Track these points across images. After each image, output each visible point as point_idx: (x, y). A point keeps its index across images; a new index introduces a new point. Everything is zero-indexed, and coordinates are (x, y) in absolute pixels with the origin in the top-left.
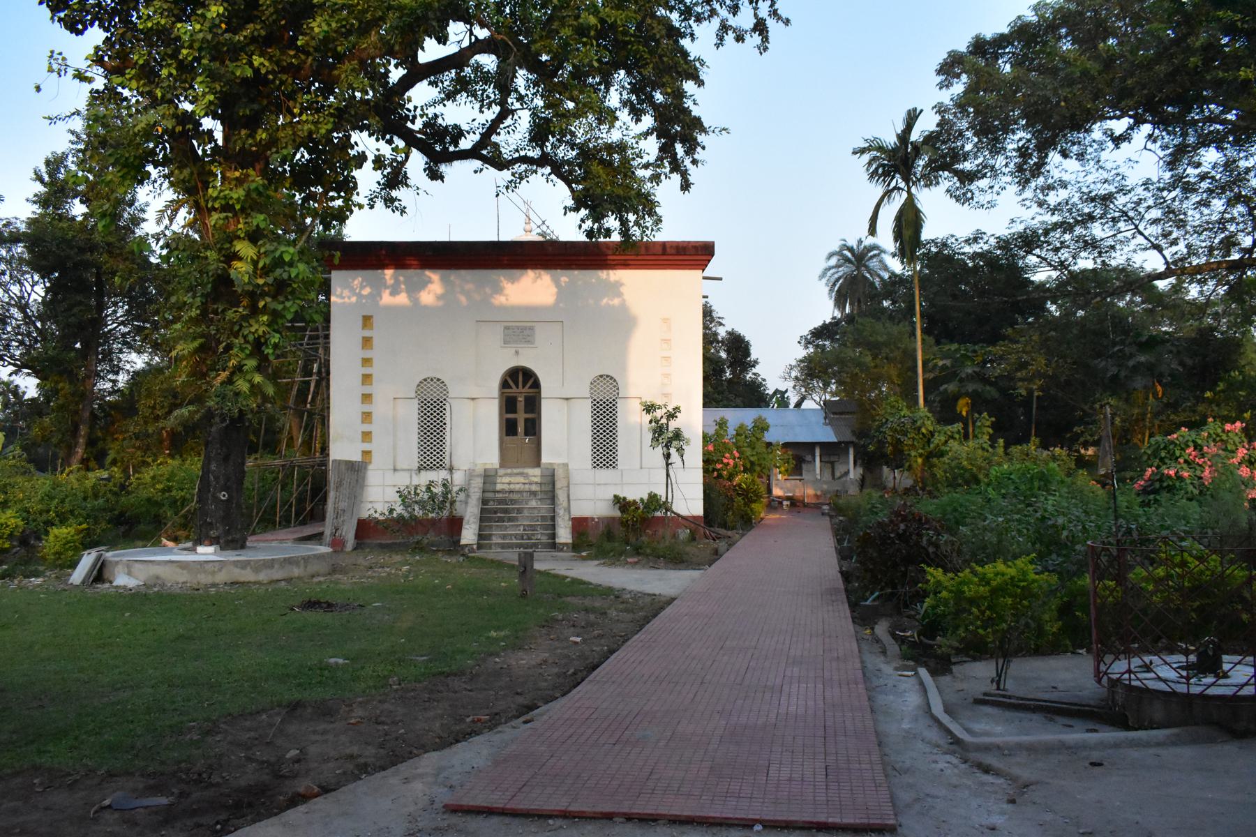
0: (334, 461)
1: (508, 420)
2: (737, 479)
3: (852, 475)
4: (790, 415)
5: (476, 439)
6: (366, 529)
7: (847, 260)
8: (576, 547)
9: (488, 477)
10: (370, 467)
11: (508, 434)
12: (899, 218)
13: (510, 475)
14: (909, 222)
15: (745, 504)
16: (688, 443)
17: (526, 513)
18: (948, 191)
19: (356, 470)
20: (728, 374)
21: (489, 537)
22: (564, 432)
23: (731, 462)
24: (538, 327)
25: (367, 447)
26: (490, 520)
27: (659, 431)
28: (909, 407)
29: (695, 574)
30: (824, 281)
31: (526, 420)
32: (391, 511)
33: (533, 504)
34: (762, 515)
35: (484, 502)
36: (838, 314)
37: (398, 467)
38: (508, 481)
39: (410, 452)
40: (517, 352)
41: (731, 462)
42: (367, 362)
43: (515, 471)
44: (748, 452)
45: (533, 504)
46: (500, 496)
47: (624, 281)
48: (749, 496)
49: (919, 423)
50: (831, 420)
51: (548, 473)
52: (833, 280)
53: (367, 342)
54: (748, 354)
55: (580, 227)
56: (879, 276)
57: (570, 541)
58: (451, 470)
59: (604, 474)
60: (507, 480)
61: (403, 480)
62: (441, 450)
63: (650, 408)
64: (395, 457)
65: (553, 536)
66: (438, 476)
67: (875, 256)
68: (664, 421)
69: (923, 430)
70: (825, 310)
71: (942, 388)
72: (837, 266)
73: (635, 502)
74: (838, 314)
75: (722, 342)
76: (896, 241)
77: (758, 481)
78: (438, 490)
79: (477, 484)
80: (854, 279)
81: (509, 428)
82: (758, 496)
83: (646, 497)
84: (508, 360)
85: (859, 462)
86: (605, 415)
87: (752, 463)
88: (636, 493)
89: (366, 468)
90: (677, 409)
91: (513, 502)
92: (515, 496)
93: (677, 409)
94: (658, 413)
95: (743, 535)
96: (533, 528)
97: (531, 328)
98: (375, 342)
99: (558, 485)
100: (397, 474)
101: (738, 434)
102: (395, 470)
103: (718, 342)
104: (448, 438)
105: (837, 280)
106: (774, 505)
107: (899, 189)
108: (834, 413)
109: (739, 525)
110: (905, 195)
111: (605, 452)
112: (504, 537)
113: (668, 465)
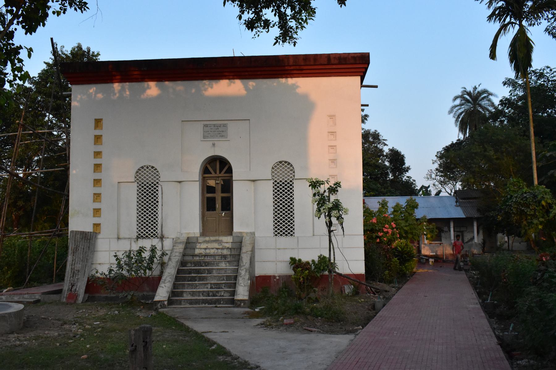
0: (72, 232)
1: (208, 199)
2: (394, 245)
3: (476, 240)
4: (431, 199)
5: (182, 214)
6: (94, 286)
7: (467, 101)
8: (253, 302)
9: (190, 243)
10: (99, 236)
11: (208, 210)
12: (513, 45)
13: (207, 242)
14: (521, 52)
15: (401, 263)
16: (346, 212)
17: (215, 274)
18: (547, 30)
19: (89, 239)
20: (391, 176)
21: (181, 294)
22: (252, 208)
23: (390, 231)
24: (231, 125)
25: (97, 220)
26: (184, 279)
27: (322, 201)
28: (528, 186)
29: (341, 341)
30: (452, 115)
31: (223, 198)
32: (111, 271)
33: (223, 265)
34: (414, 270)
35: (183, 263)
36: (461, 137)
37: (121, 236)
38: (206, 247)
39: (130, 225)
40: (214, 145)
41: (390, 231)
42: (97, 154)
43: (212, 238)
44: (403, 224)
45: (223, 265)
46: (197, 258)
47: (299, 84)
48: (405, 256)
49: (539, 197)
50: (460, 202)
51: (237, 240)
52: (458, 113)
53: (98, 139)
54: (404, 164)
55: (240, 18)
56: (488, 110)
57: (246, 298)
58: (162, 238)
59: (283, 241)
60: (204, 246)
61: (124, 247)
62: (155, 222)
63: (315, 184)
64: (118, 229)
65: (233, 293)
66: (147, 244)
67: (485, 97)
68: (326, 194)
69: (543, 203)
70: (452, 134)
71: (549, 174)
72: (461, 105)
73: (308, 263)
74: (461, 137)
75: (386, 156)
76: (511, 62)
77: (410, 245)
78: (146, 255)
79: (180, 248)
80: (472, 110)
81: (208, 205)
82: (410, 256)
83: (316, 259)
84: (208, 151)
85: (481, 232)
86: (283, 193)
87: (406, 232)
88: (309, 256)
89: (96, 238)
90: (338, 184)
91: (207, 264)
92: (207, 259)
93: (338, 184)
94: (322, 189)
95: (399, 288)
96: (218, 286)
97: (225, 126)
98: (104, 139)
99: (244, 250)
100: (120, 241)
101: (394, 211)
102: (118, 238)
103: (383, 156)
104: (159, 213)
105: (461, 114)
106: (423, 261)
107: (512, 23)
108: (464, 199)
109: (395, 280)
110: (517, 27)
111: (284, 224)
112: (193, 294)
113: (330, 232)
